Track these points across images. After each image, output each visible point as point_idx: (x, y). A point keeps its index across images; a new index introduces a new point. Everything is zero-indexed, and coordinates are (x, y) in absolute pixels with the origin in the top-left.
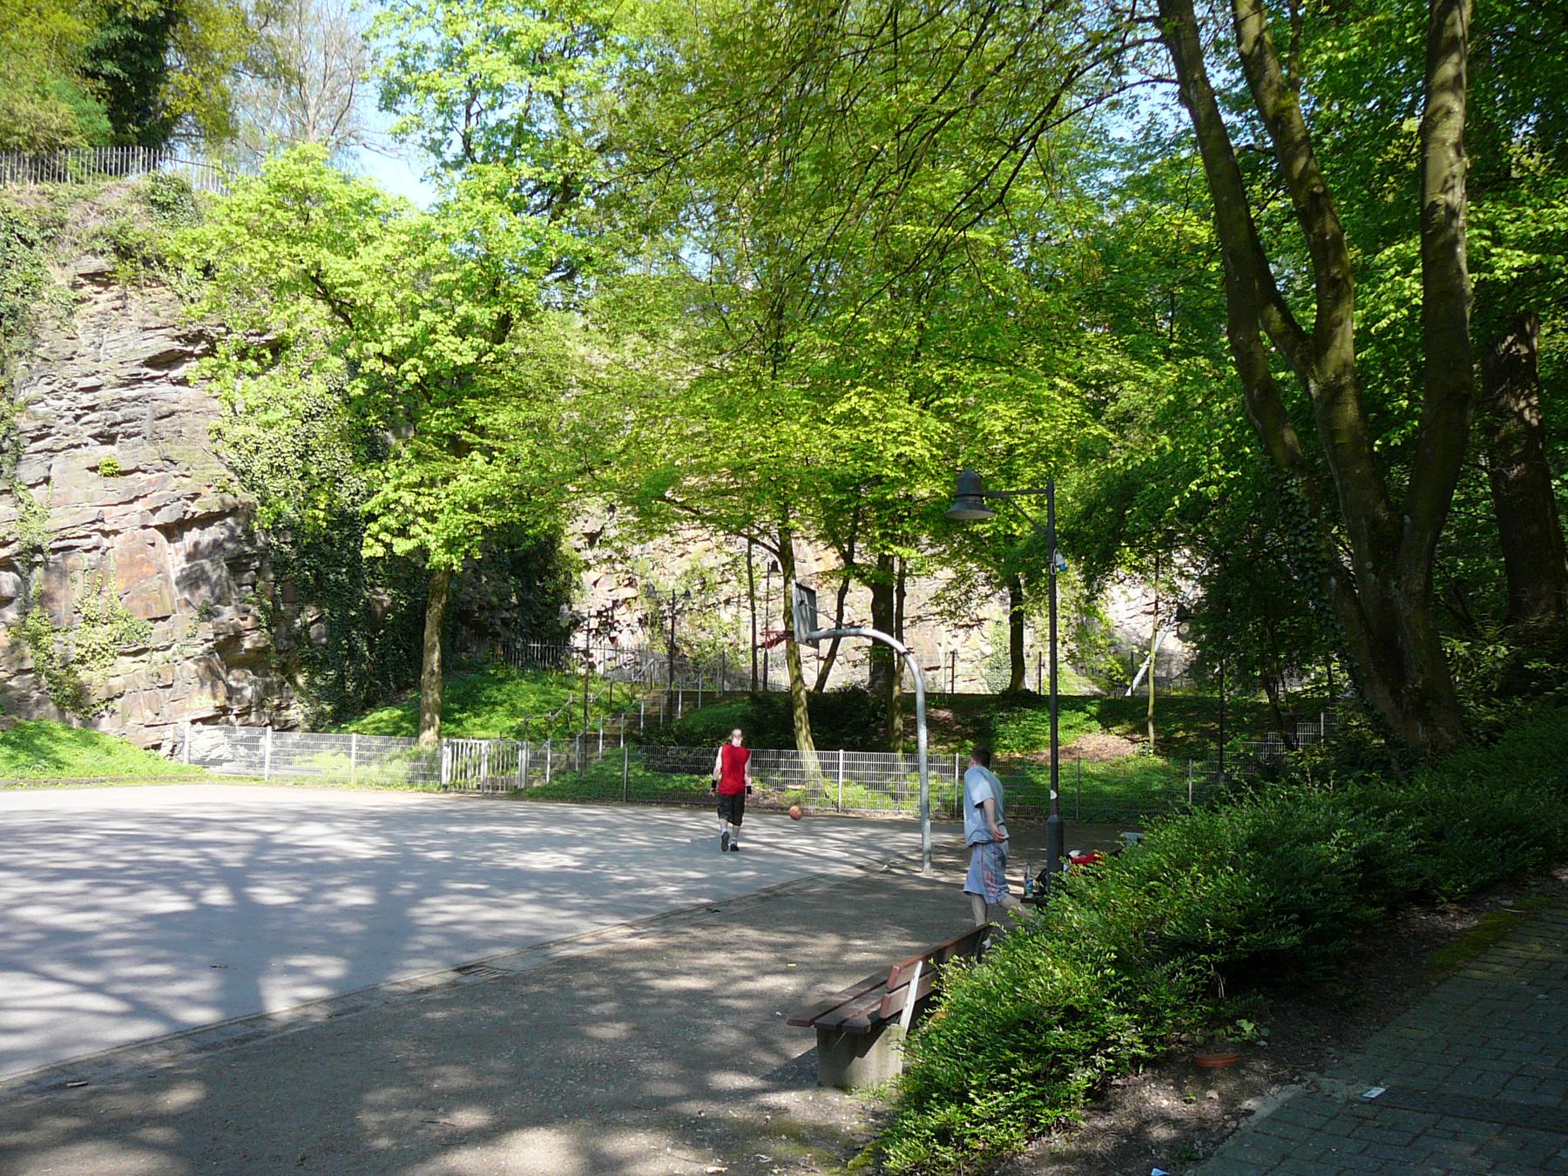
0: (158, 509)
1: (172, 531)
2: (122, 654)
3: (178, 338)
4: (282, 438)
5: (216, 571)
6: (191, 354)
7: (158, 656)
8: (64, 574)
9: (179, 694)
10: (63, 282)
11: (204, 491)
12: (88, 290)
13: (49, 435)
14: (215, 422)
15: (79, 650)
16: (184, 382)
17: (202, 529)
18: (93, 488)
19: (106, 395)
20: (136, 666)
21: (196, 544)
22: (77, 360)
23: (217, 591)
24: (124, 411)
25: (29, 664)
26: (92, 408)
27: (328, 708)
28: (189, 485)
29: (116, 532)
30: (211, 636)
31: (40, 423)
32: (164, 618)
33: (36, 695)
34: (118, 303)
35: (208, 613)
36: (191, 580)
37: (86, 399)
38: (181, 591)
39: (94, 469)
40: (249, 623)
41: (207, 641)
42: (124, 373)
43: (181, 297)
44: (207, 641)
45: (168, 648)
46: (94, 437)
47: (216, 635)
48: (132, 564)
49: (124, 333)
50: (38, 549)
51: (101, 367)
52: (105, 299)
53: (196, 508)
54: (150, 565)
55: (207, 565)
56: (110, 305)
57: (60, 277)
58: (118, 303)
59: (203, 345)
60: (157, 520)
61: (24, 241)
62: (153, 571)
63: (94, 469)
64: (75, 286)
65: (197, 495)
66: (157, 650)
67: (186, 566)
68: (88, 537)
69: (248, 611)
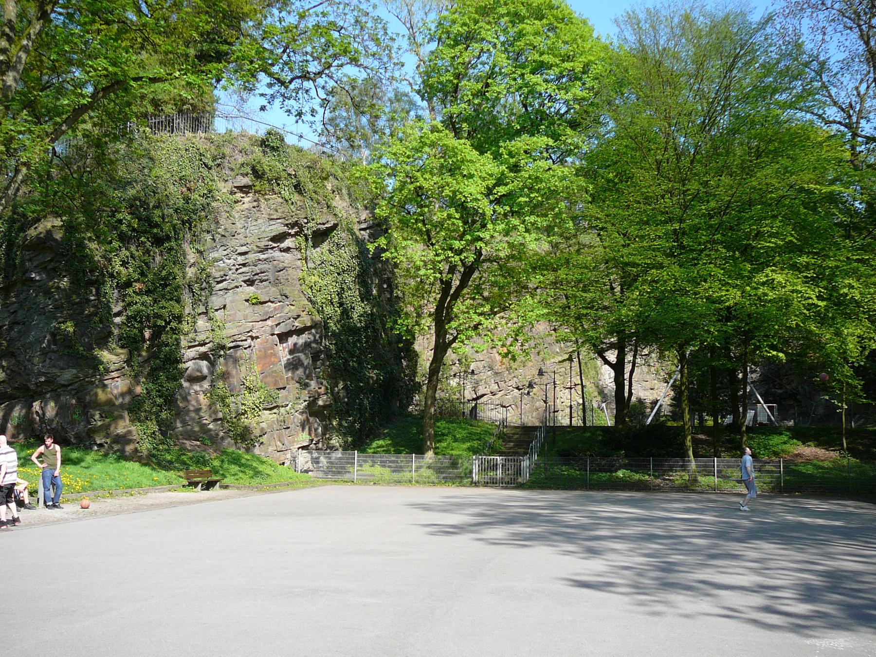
0: (279, 324)
1: (283, 337)
2: (265, 409)
3: (287, 225)
4: (329, 285)
5: (307, 361)
6: (289, 234)
7: (282, 410)
8: (236, 361)
10: (225, 190)
11: (303, 314)
12: (239, 195)
13: (225, 280)
14: (301, 275)
15: (244, 407)
16: (287, 250)
17: (298, 336)
18: (247, 311)
19: (252, 257)
20: (271, 416)
21: (295, 344)
22: (236, 237)
23: (307, 372)
24: (260, 266)
25: (220, 415)
26: (244, 265)
27: (350, 439)
29: (257, 337)
31: (222, 273)
32: (284, 388)
33: (221, 434)
34: (255, 204)
36: (292, 366)
37: (241, 259)
38: (287, 371)
39: (247, 301)
40: (322, 390)
42: (262, 244)
43: (287, 201)
44: (305, 401)
46: (245, 281)
48: (266, 356)
49: (260, 221)
50: (223, 347)
51: (248, 240)
52: (248, 200)
55: (302, 356)
56: (251, 205)
57: (223, 188)
58: (255, 204)
59: (296, 229)
61: (206, 166)
63: (247, 301)
64: (232, 193)
65: (299, 316)
67: (289, 357)
68: (246, 340)
69: (322, 384)
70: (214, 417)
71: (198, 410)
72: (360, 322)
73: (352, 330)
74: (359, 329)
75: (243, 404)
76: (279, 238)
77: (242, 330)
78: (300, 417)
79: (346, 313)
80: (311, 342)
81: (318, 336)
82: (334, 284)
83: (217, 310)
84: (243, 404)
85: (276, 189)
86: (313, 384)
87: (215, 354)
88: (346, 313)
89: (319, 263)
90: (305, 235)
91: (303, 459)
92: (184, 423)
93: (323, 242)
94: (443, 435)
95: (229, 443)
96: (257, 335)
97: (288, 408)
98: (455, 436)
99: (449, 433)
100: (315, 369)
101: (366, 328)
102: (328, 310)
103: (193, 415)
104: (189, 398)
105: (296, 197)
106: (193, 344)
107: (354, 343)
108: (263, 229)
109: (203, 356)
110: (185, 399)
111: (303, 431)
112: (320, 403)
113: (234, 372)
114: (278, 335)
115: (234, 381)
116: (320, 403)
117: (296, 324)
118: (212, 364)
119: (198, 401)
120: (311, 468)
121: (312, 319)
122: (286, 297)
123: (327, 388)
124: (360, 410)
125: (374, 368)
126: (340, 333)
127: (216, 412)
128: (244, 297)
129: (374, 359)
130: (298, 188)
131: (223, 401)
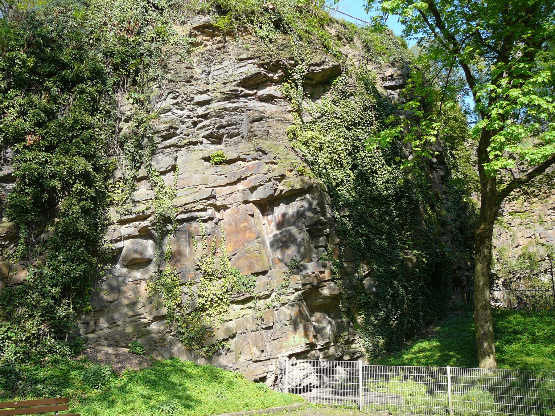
2: (233, 302)
4: (335, 140)
5: (300, 235)
7: (261, 303)
9: (278, 334)
15: (200, 300)
16: (270, 99)
17: (287, 204)
18: (207, 173)
19: (215, 106)
21: (284, 215)
22: (193, 83)
24: (227, 118)
25: (164, 311)
26: (205, 117)
27: (382, 341)
28: (277, 171)
29: (225, 208)
30: (300, 286)
32: (264, 273)
35: (296, 268)
36: (282, 243)
37: (200, 111)
40: (327, 275)
41: (297, 290)
44: (297, 290)
45: (268, 296)
47: (304, 285)
48: (237, 232)
49: (225, 63)
53: (283, 187)
54: (251, 232)
55: (294, 230)
58: (220, 45)
59: (280, 73)
60: (254, 197)
61: (157, 8)
62: (253, 236)
65: (283, 177)
66: (260, 298)
68: (204, 210)
70: (155, 313)
71: (133, 305)
72: (387, 189)
73: (379, 200)
74: (386, 198)
75: (200, 296)
76: (252, 83)
77: (198, 197)
78: (288, 312)
79: (364, 178)
80: (304, 211)
81: (315, 202)
82: (341, 140)
83: (164, 173)
84: (200, 296)
85: (249, 26)
86: (311, 267)
87: (162, 227)
88: (364, 178)
89: (318, 115)
90: (294, 81)
91: (301, 372)
92: (113, 323)
93: (324, 92)
94: (515, 332)
95: (179, 350)
96: (225, 203)
97: (269, 300)
98: (533, 334)
99: (525, 330)
100: (317, 247)
101: (398, 197)
102: (339, 174)
103: (125, 310)
104: (124, 288)
105: (278, 36)
106: (128, 217)
107: (380, 216)
108: (230, 73)
109: (145, 234)
110: (116, 289)
111: (295, 328)
112: (326, 292)
113: (186, 250)
114: (254, 203)
115: (188, 263)
116: (326, 292)
117: (280, 187)
118: (159, 244)
119: (136, 292)
120: (316, 383)
121: (302, 180)
122: (263, 152)
123: (332, 273)
124: (394, 301)
125: (415, 247)
126: (356, 203)
127: (160, 305)
128: (201, 155)
129: (413, 238)
130: (278, 25)
131: (169, 291)
